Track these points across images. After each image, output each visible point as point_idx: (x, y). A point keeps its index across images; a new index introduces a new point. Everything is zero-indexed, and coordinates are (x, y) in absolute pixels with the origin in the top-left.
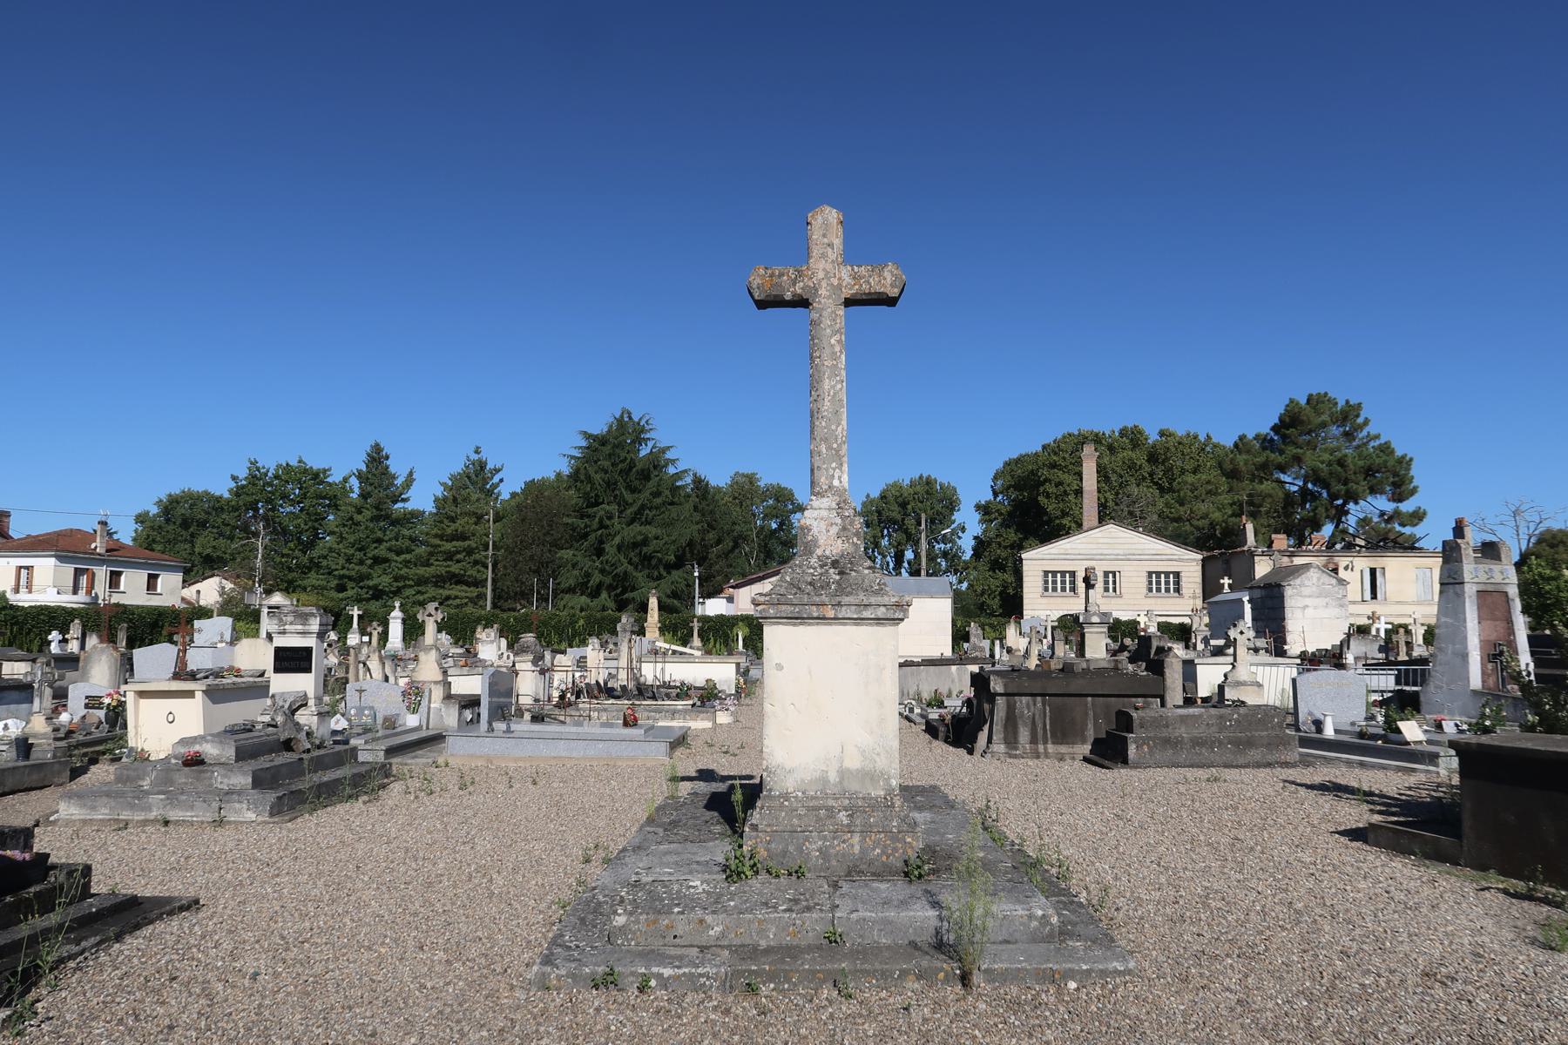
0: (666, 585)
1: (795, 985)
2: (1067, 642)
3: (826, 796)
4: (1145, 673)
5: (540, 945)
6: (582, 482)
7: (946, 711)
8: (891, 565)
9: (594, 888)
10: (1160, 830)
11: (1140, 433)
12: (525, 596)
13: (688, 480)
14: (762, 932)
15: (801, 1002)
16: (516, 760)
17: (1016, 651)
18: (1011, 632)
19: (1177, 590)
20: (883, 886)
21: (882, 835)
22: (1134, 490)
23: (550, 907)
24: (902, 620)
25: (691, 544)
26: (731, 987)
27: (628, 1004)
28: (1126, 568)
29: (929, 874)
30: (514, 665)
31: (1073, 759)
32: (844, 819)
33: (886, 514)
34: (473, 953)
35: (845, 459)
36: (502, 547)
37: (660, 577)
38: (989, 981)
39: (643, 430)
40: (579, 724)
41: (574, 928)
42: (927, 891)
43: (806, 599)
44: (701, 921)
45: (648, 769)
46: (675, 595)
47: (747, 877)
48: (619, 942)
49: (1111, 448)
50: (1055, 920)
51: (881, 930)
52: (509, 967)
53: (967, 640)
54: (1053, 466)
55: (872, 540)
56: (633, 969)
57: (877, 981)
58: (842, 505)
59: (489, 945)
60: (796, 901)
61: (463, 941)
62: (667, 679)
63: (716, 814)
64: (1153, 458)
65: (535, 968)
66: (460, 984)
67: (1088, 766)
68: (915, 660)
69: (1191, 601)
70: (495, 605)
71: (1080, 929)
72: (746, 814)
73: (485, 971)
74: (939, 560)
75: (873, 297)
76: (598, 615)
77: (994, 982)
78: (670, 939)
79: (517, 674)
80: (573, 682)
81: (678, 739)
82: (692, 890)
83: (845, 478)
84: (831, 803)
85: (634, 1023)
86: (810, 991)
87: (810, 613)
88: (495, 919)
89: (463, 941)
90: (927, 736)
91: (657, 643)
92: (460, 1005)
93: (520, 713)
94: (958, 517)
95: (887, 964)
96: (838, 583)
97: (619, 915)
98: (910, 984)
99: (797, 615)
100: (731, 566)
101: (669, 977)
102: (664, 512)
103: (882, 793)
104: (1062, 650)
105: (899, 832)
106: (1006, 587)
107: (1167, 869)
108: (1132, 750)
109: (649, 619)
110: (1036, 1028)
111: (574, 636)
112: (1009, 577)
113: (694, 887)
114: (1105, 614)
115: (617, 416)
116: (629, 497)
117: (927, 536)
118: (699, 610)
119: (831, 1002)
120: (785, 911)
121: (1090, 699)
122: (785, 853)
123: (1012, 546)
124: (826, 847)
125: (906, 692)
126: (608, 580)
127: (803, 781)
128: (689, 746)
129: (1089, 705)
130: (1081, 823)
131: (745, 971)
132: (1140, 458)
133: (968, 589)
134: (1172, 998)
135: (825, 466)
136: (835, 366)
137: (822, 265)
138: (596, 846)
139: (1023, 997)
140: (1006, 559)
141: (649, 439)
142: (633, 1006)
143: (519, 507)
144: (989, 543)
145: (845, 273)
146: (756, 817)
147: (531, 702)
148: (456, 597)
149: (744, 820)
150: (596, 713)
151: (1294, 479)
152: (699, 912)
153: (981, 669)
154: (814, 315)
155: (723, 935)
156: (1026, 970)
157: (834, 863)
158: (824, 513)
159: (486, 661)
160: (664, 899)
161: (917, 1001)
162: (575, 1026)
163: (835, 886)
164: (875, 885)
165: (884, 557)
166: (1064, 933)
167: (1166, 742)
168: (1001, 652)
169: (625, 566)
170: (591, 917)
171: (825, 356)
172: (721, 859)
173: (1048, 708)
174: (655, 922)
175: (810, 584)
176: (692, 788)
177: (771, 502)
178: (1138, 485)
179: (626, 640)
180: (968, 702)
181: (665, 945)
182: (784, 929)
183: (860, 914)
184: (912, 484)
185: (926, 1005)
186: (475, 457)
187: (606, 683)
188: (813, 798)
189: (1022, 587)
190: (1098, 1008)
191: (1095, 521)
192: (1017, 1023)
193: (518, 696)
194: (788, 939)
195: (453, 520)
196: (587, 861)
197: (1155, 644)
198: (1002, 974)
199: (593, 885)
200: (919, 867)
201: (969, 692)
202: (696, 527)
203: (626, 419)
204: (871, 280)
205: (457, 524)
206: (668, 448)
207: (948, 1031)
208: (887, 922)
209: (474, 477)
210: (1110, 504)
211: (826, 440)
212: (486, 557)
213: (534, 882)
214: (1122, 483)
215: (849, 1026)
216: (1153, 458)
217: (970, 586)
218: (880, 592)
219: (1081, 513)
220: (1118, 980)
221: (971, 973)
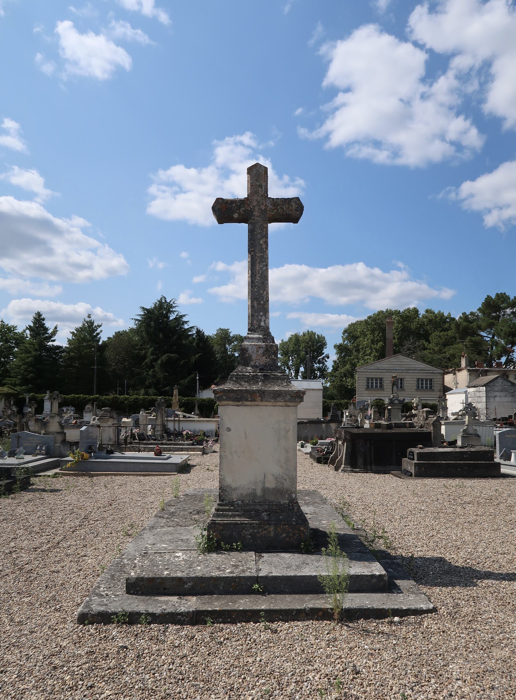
8: (293, 374)
19: (431, 388)
21: (287, 526)
28: (407, 377)
32: (265, 516)
39: (172, 307)
41: (107, 582)
57: (283, 616)
68: (305, 421)
69: (438, 393)
82: (176, 559)
94: (326, 351)
105: (297, 524)
113: (178, 557)
127: (242, 494)
135: (256, 314)
151: (488, 335)
165: (290, 370)
170: (118, 574)
186: (88, 319)
188: (248, 505)
204: (284, 207)
206: (184, 316)
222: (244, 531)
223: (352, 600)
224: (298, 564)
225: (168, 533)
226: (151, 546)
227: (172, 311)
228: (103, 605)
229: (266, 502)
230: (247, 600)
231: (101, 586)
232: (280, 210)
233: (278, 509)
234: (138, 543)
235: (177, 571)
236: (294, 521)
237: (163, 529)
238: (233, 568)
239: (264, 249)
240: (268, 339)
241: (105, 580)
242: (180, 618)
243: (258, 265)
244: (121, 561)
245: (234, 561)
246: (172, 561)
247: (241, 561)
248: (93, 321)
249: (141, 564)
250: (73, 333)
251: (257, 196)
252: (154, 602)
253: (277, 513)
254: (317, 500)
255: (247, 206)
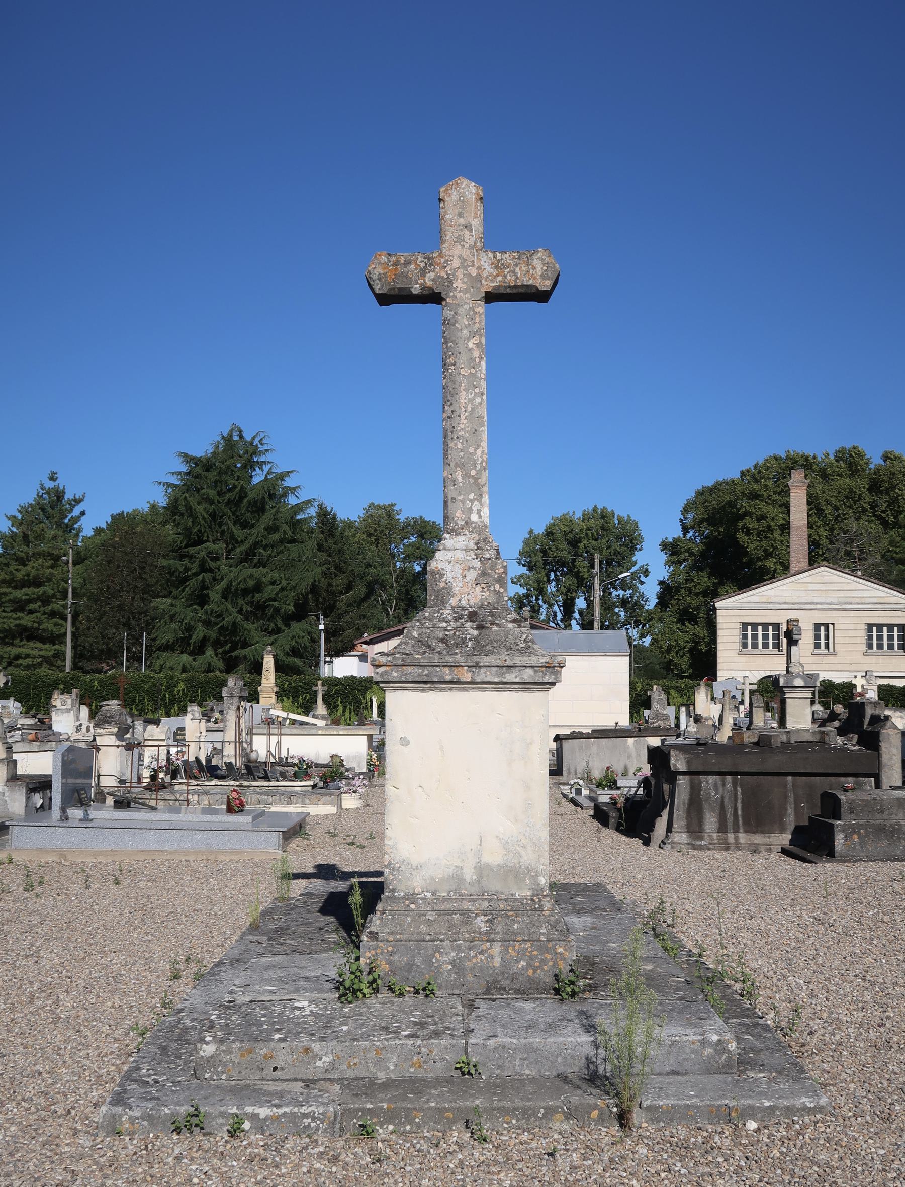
0: (285, 640)
1: (419, 1126)
2: (768, 709)
3: (461, 898)
4: (856, 748)
5: (113, 1080)
6: (182, 515)
7: (619, 792)
8: (559, 616)
9: (181, 1011)
10: (868, 936)
11: (860, 455)
12: (111, 654)
13: (312, 511)
14: (380, 1062)
15: (425, 1147)
16: (95, 854)
17: (707, 719)
18: (701, 697)
20: (529, 1006)
21: (528, 944)
22: (853, 525)
23: (127, 1034)
24: (553, 684)
25: (314, 589)
26: (342, 1129)
27: (216, 1152)
29: (584, 991)
30: (94, 740)
31: (770, 850)
32: (482, 925)
33: (552, 553)
34: (30, 1092)
35: (486, 489)
36: (84, 595)
37: (278, 631)
38: (654, 1120)
40: (177, 811)
42: (582, 1013)
43: (436, 659)
44: (307, 1050)
45: (256, 864)
46: (295, 652)
47: (364, 996)
48: (207, 1076)
49: (824, 475)
50: (733, 1046)
51: (525, 1059)
52: (73, 1108)
53: (648, 707)
54: (754, 496)
55: (536, 585)
56: (222, 1109)
57: (518, 1120)
58: (482, 545)
59: (50, 1081)
60: (422, 1025)
61: (18, 1077)
62: (284, 754)
63: (332, 919)
64: (875, 486)
65: (104, 1109)
66: (12, 1129)
67: (788, 859)
68: (584, 731)
70: (75, 667)
71: (764, 1057)
72: (365, 920)
73: (44, 1113)
74: (617, 610)
75: (521, 290)
76: (202, 677)
77: (659, 1122)
78: (268, 1072)
79: (98, 750)
80: (168, 759)
81: (294, 828)
82: (297, 1013)
83: (485, 512)
84: (467, 905)
85: (221, 1174)
86: (437, 1133)
87: (442, 677)
88: (60, 1049)
89: (18, 1077)
90: (596, 823)
91: (272, 712)
92: (11, 1154)
93: (101, 797)
94: (640, 558)
95: (529, 1100)
96: (476, 639)
97: (207, 1043)
98: (558, 1124)
99: (425, 679)
100: (364, 617)
101: (265, 1119)
102: (282, 552)
103: (529, 894)
104: (761, 719)
105: (549, 941)
106: (697, 643)
107: (873, 984)
108: (839, 841)
109: (264, 682)
110: (706, 1178)
111: (172, 703)
112: (703, 633)
113: (300, 1008)
114: (810, 676)
115: (225, 435)
116: (238, 532)
117: (602, 581)
118: (326, 671)
119: (461, 1146)
120: (409, 1036)
121: (790, 778)
122: (410, 966)
123: (705, 593)
124: (460, 958)
125: (572, 771)
126: (213, 634)
127: (432, 879)
128: (307, 836)
129: (790, 786)
130: (773, 928)
131: (359, 1110)
132: (861, 485)
133: (652, 644)
134: (870, 1141)
135: (461, 497)
136: (473, 375)
137: (457, 251)
138: (188, 959)
139: (693, 1140)
140: (698, 608)
141: (264, 462)
142: (222, 1153)
143: (104, 545)
144: (678, 589)
145: (485, 261)
146: (375, 923)
147: (115, 784)
148: (28, 656)
149: (363, 925)
150: (196, 798)
152: (304, 1038)
153: (663, 741)
154: (448, 313)
155: (333, 1066)
156: (697, 1107)
157: (470, 978)
158: (460, 555)
159: (60, 734)
160: (261, 1024)
161: (565, 1144)
162: (149, 1179)
163: (471, 1006)
164: (520, 1004)
165: (551, 605)
166: (744, 1062)
167: (881, 831)
168: (688, 722)
169: (233, 616)
170: (174, 1045)
171: (461, 363)
172: (333, 974)
173: (739, 789)
174: (250, 1052)
175: (442, 640)
176: (306, 888)
177: (413, 539)
178: (858, 519)
179: (234, 708)
180: (645, 782)
181: (263, 1080)
182: (406, 1059)
183: (499, 1040)
184: (586, 518)
185: (575, 1150)
186: (50, 484)
187: (209, 760)
188: (445, 900)
189: (715, 643)
190: (781, 1153)
191: (805, 563)
192: (683, 1171)
193: (99, 776)
194: (412, 1070)
195: (23, 562)
196: (176, 977)
197: (869, 712)
198: (668, 1112)
199: (180, 1006)
200: (572, 983)
201: (647, 770)
202: (319, 570)
203: (236, 438)
204: (517, 270)
205: (28, 568)
206: (288, 473)
207: (600, 1180)
208: (531, 1049)
209: (49, 509)
210: (824, 542)
211: (462, 466)
212: (65, 606)
213: (109, 1004)
214: (838, 516)
215: (482, 1176)
216: (875, 486)
217: (654, 641)
218: (527, 650)
219: (789, 553)
220: (807, 1119)
221: (630, 1111)
222: (437, 955)
223: (661, 1088)
224: (550, 1021)
225: (274, 966)
226: (242, 989)
227: (258, 462)
228: (151, 1099)
229: (483, 895)
230: (446, 1089)
231: (141, 1066)
232: (509, 277)
233: (509, 908)
234: (209, 990)
235: (300, 1033)
236: (543, 934)
237: (264, 960)
238: (416, 1027)
239: (477, 360)
240: (487, 550)
241: (149, 1057)
242: (309, 1123)
243: (464, 393)
244: (179, 1023)
245: (418, 1015)
246: (288, 1016)
247: (433, 1016)
248: (61, 488)
249: (223, 1021)
250: (13, 518)
251: (460, 247)
252: (254, 1094)
253: (508, 917)
254: (602, 904)
255: (441, 269)
